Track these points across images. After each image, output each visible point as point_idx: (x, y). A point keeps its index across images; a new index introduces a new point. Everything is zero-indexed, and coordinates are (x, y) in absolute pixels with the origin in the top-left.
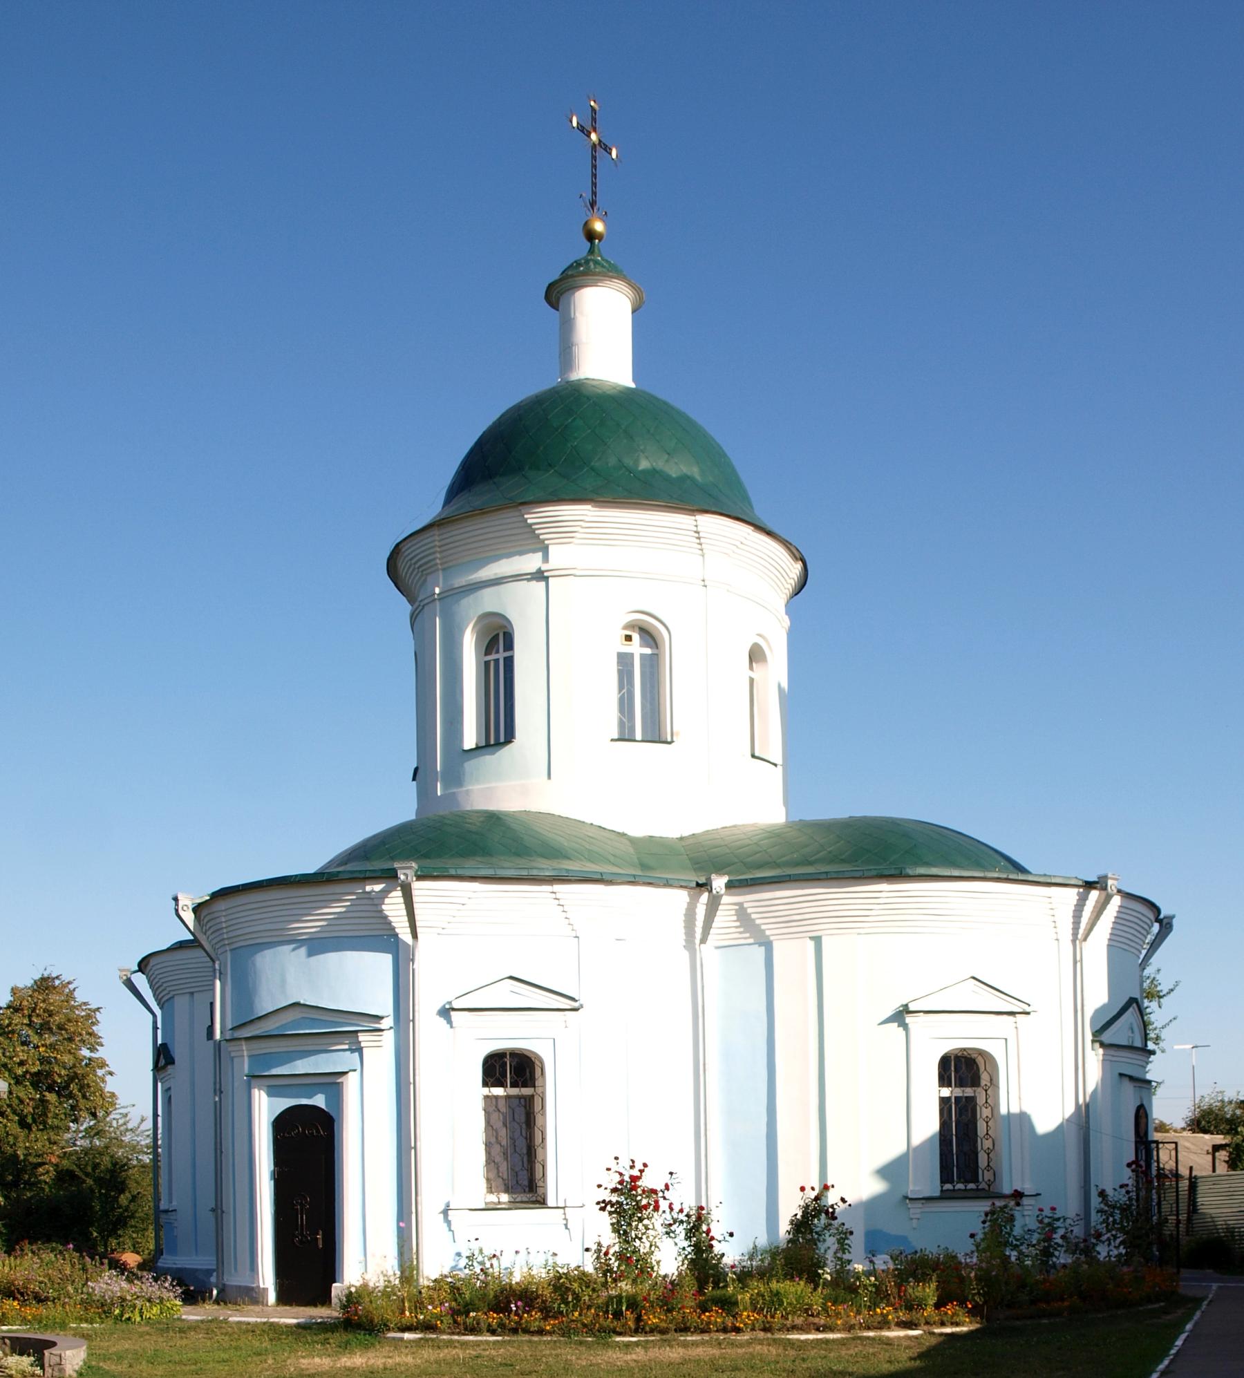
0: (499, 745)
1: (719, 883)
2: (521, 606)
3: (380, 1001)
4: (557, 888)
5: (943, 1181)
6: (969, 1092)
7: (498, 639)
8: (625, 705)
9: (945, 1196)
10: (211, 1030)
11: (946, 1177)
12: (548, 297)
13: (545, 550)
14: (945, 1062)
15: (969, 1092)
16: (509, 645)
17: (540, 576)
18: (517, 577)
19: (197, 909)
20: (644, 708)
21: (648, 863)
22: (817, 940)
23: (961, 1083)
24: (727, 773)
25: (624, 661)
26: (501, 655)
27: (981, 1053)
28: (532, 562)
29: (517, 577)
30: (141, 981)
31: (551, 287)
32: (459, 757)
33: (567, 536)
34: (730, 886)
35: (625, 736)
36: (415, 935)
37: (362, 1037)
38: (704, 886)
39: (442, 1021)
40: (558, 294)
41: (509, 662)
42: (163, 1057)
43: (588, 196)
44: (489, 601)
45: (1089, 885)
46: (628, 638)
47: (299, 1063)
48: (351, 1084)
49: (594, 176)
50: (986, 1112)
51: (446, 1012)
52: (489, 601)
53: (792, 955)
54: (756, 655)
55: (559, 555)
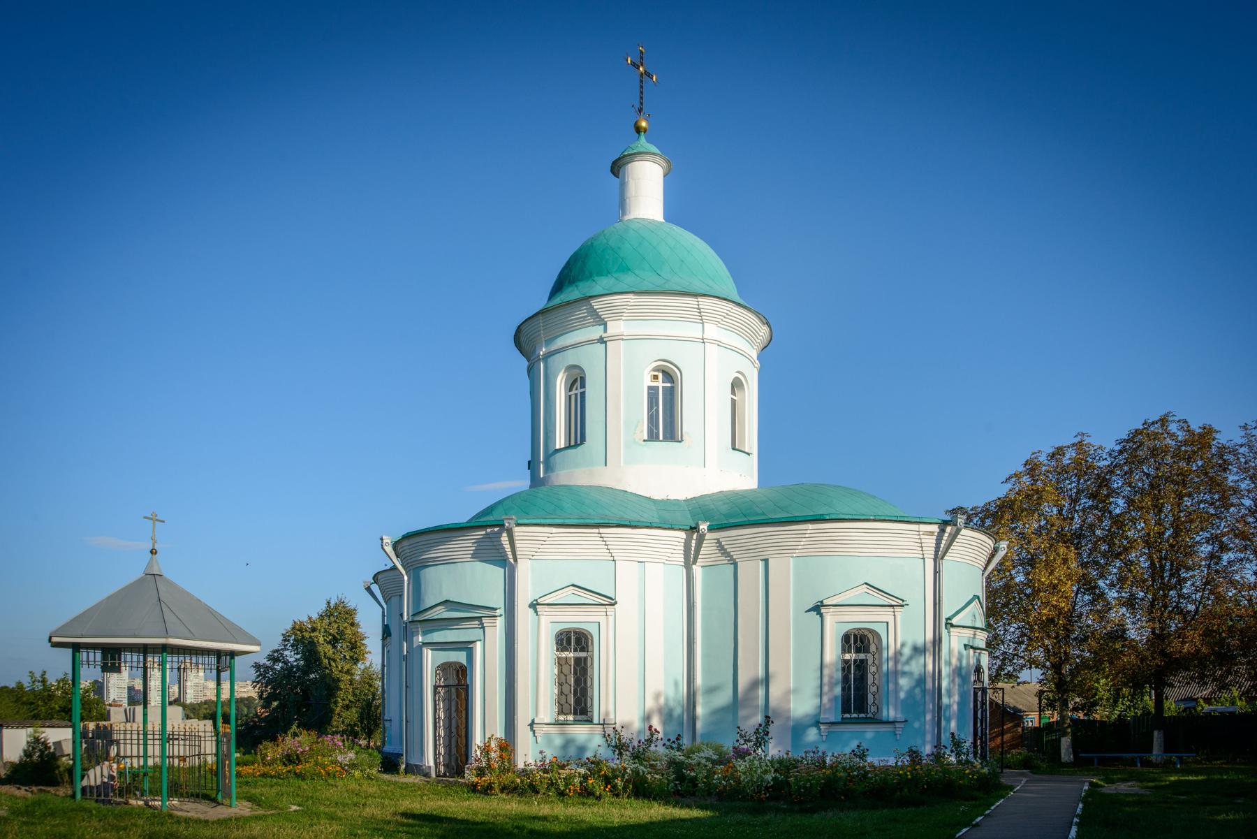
0: (576, 445)
1: (703, 527)
2: (589, 359)
3: (497, 600)
4: (602, 530)
5: (844, 651)
6: (862, 656)
7: (577, 381)
8: (653, 420)
9: (844, 722)
10: (402, 615)
11: (845, 708)
12: (612, 171)
13: (605, 324)
14: (846, 638)
15: (862, 656)
16: (583, 386)
17: (602, 340)
18: (589, 342)
19: (395, 546)
20: (665, 419)
21: (659, 516)
22: (766, 561)
23: (858, 651)
24: (715, 461)
25: (653, 392)
26: (579, 391)
27: (871, 631)
28: (597, 332)
29: (589, 342)
30: (375, 588)
31: (614, 163)
32: (552, 453)
33: (618, 316)
34: (710, 529)
35: (653, 437)
36: (516, 560)
37: (484, 620)
38: (694, 529)
39: (531, 611)
40: (617, 168)
41: (583, 394)
42: (386, 632)
43: (637, 105)
44: (571, 358)
45: (946, 523)
46: (656, 377)
47: (435, 634)
48: (478, 647)
49: (642, 87)
50: (873, 669)
51: (534, 606)
52: (571, 358)
53: (750, 571)
54: (736, 385)
55: (614, 328)
